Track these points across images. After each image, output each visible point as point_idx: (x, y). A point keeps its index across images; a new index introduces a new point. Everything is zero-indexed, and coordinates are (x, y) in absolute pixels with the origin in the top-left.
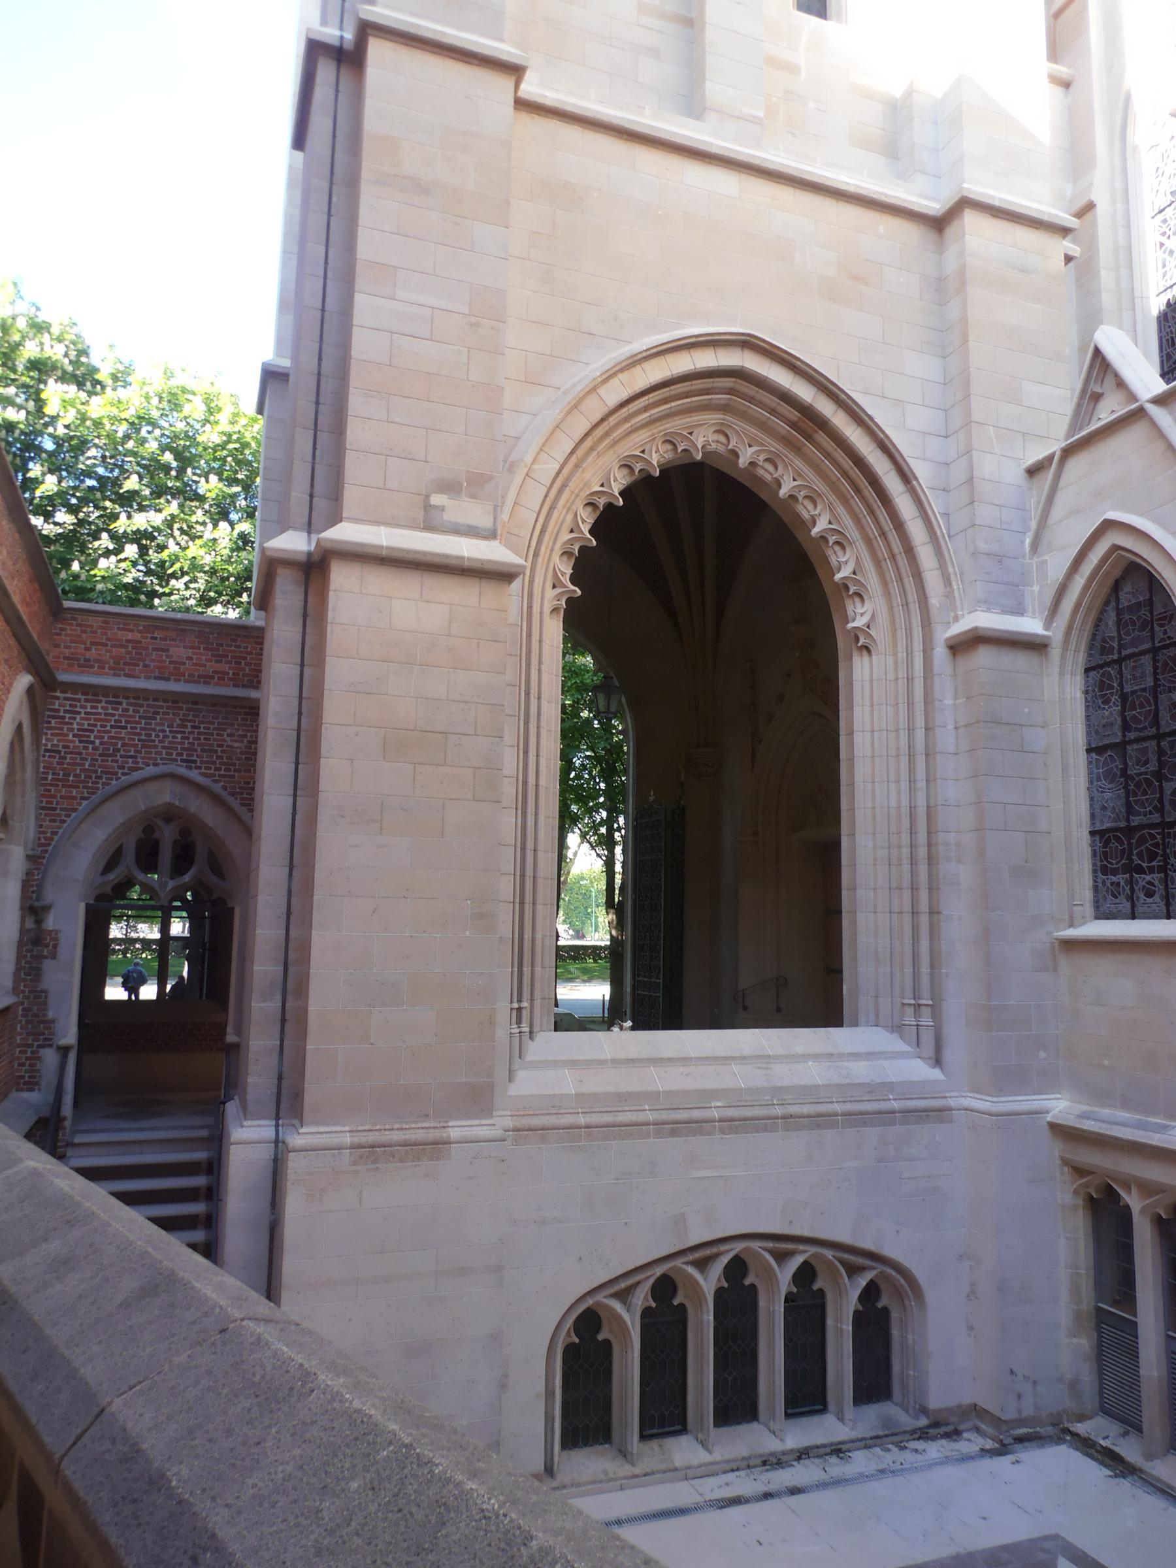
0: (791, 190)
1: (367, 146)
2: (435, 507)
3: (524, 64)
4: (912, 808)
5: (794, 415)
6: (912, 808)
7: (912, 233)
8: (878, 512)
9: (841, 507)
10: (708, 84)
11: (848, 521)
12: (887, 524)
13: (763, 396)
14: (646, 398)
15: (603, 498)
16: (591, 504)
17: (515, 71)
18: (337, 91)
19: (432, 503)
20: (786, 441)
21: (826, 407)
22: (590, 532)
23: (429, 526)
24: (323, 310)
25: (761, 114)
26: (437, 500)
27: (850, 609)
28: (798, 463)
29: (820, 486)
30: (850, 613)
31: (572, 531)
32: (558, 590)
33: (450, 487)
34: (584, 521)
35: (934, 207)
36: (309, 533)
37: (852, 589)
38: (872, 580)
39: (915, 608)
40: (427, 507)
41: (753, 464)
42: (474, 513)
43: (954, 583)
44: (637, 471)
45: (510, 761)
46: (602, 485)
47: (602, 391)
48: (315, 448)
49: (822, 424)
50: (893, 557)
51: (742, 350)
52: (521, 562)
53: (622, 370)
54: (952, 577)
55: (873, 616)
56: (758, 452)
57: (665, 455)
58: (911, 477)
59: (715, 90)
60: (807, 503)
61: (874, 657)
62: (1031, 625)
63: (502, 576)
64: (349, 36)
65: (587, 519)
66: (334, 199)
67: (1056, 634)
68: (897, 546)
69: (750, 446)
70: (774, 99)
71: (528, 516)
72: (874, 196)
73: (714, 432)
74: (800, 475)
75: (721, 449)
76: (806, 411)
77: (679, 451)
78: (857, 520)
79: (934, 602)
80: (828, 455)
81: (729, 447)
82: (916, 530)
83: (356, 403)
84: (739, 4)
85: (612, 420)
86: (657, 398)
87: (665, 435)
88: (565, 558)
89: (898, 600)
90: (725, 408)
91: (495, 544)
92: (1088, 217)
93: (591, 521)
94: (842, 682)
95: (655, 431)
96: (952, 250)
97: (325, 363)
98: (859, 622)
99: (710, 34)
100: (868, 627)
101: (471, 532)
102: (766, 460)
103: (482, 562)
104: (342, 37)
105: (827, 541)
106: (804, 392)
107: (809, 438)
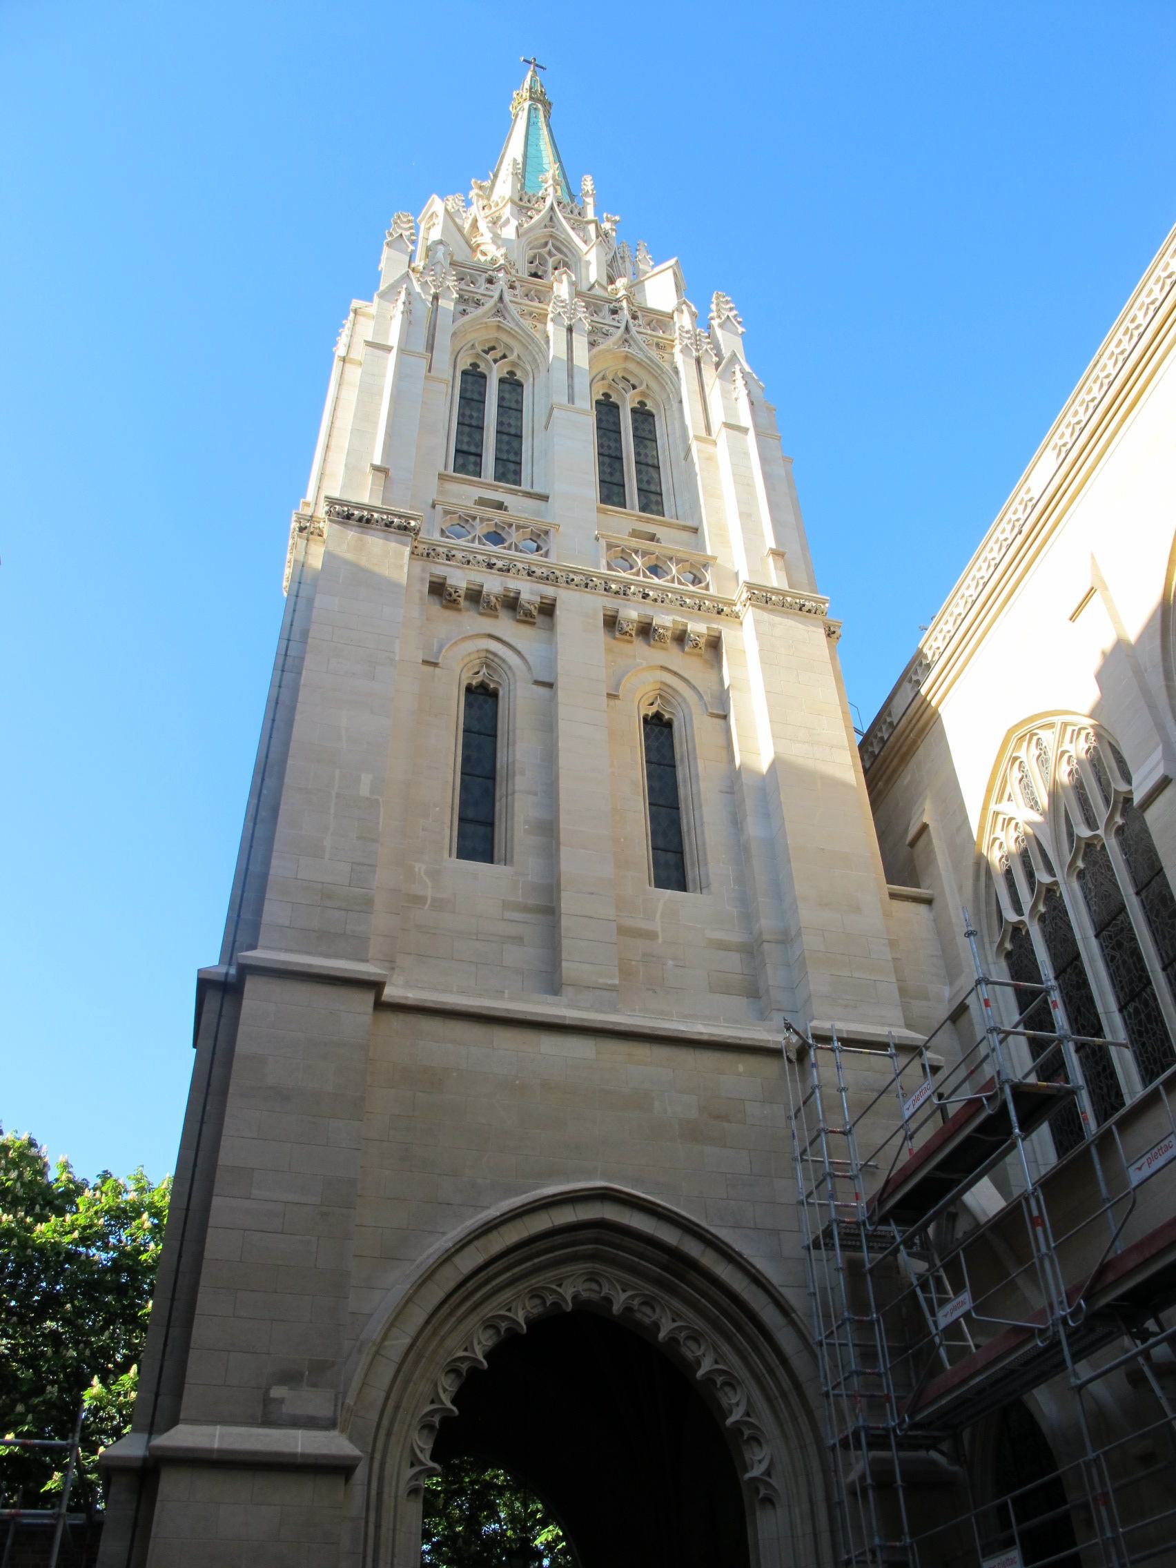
0: (648, 1045)
1: (236, 1065)
2: (275, 1400)
3: (381, 980)
5: (665, 1258)
9: (726, 1344)
10: (564, 964)
11: (734, 1359)
12: (774, 1360)
13: (628, 1242)
14: (506, 1259)
15: (466, 1364)
16: (453, 1370)
17: (376, 986)
18: (220, 1016)
19: (271, 1396)
20: (659, 1282)
21: (693, 1248)
22: (434, 1458)
23: (267, 1421)
24: (187, 1209)
25: (616, 982)
26: (277, 1392)
27: (747, 1456)
28: (676, 1304)
29: (700, 1324)
32: (417, 1469)
33: (290, 1378)
34: (445, 1390)
36: (150, 1434)
37: (747, 1433)
38: (765, 1419)
39: (803, 1419)
40: (267, 1401)
41: (628, 1309)
42: (315, 1402)
44: (503, 1331)
46: (466, 1350)
47: (457, 1260)
48: (165, 1345)
49: (693, 1265)
50: (784, 1395)
51: (602, 1202)
52: (356, 1452)
53: (477, 1237)
56: (632, 1297)
57: (532, 1311)
59: (569, 968)
60: (690, 1343)
63: (340, 1469)
64: (233, 971)
65: (447, 1388)
66: (208, 1108)
69: (624, 1291)
70: (633, 963)
71: (376, 1394)
72: (728, 1041)
74: (678, 1315)
75: (595, 1297)
76: (675, 1254)
80: (704, 1295)
81: (602, 1295)
83: (204, 1300)
84: (592, 894)
86: (501, 1267)
87: (532, 1290)
88: (425, 1432)
90: (592, 1257)
91: (334, 1433)
92: (963, 1021)
93: (453, 1389)
94: (751, 1543)
95: (521, 1287)
97: (183, 1260)
98: (757, 1472)
99: (565, 922)
101: (310, 1423)
102: (643, 1303)
103: (316, 1456)
104: (227, 974)
105: (714, 1382)
107: (682, 1279)
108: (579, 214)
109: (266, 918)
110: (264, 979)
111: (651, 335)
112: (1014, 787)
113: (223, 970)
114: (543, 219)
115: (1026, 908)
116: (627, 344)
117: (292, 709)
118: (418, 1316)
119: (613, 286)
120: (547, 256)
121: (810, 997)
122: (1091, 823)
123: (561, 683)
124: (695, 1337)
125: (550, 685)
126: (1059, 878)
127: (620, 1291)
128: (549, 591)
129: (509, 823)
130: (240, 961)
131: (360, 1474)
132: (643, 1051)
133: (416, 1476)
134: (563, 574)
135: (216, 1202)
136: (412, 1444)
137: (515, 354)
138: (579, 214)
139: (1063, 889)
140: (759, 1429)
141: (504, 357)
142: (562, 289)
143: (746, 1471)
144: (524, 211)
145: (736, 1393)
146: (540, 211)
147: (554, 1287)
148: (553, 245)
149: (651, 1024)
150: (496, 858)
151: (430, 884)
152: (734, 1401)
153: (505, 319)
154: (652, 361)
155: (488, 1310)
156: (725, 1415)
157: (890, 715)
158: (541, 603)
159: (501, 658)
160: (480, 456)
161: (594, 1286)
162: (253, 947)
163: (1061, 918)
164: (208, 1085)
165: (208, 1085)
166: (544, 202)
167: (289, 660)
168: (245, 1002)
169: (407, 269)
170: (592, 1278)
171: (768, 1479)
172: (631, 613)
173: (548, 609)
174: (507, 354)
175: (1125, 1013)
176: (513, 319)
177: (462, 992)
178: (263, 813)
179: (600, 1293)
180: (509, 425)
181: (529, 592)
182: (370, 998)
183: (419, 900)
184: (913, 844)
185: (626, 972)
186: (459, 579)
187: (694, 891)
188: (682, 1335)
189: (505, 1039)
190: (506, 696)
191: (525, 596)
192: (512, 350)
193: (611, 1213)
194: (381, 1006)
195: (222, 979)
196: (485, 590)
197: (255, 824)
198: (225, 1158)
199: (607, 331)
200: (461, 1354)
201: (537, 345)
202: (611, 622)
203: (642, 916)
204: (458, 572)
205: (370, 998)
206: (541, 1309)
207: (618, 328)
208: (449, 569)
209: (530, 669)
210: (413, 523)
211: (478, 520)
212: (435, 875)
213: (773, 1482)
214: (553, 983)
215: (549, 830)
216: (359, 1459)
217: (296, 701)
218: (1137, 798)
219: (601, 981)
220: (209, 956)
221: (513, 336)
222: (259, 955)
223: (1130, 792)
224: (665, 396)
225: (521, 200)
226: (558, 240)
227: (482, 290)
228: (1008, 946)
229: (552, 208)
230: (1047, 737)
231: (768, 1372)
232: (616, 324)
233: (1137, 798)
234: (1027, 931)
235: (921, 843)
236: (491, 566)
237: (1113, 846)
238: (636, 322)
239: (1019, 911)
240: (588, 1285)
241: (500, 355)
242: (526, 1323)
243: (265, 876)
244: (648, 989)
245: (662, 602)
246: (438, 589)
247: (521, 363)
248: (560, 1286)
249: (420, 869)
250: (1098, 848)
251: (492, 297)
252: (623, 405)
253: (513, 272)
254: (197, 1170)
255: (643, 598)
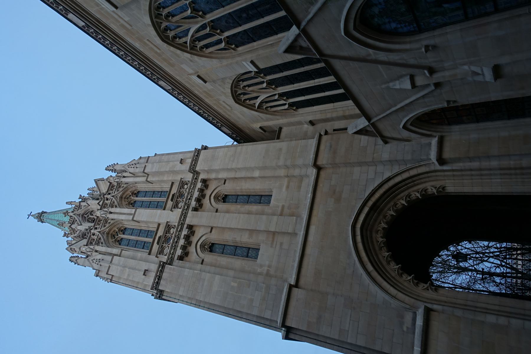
4: (501, 174)
6: (501, 174)
7: (322, 173)
8: (420, 178)
11: (402, 195)
12: (403, 183)
16: (401, 275)
17: (291, 287)
18: (296, 334)
21: (370, 203)
22: (426, 283)
28: (386, 209)
29: (392, 203)
30: (432, 193)
31: (410, 282)
35: (315, 171)
37: (424, 193)
39: (429, 175)
42: (408, 317)
43: (421, 164)
45: (491, 319)
49: (375, 204)
54: (419, 165)
55: (432, 186)
56: (383, 221)
58: (389, 178)
60: (397, 206)
61: (446, 186)
62: (434, 142)
63: (428, 312)
64: (283, 329)
67: (438, 134)
68: (410, 180)
69: (381, 224)
73: (378, 235)
76: (371, 209)
77: (383, 246)
78: (403, 191)
79: (427, 169)
82: (405, 175)
85: (377, 267)
89: (427, 179)
96: (326, 166)
100: (436, 187)
104: (284, 331)
106: (366, 210)
108: (77, 206)
109: (269, 318)
110: (286, 320)
111: (115, 190)
112: (252, 102)
113: (283, 331)
114: (77, 217)
115: (285, 102)
116: (117, 197)
117: (211, 304)
118: (385, 284)
119: (100, 199)
120: (89, 217)
121: (304, 164)
122: (263, 83)
123: (211, 225)
124: (395, 204)
125: (212, 228)
126: (277, 93)
127: (381, 225)
128: (185, 226)
129: (249, 243)
130: (281, 326)
131: (429, 306)
132: (315, 212)
133: (432, 289)
134: (181, 222)
135: (349, 341)
136: (423, 289)
137: (116, 229)
138: (77, 206)
139: (280, 92)
140: (422, 190)
141: (117, 232)
142: (98, 214)
143: (434, 194)
144: (74, 223)
145: (428, 189)
146: (75, 218)
147: (379, 243)
148: (85, 215)
149: (307, 209)
150: (259, 248)
151: (264, 268)
152: (414, 195)
153: (106, 231)
154: (123, 190)
155: (384, 263)
156: (418, 198)
157: (230, 134)
158: (188, 229)
159: (203, 242)
160: (145, 242)
161: (379, 232)
162: (277, 322)
163: (288, 93)
164: (315, 339)
165: (315, 339)
166: (72, 216)
167: (197, 304)
168: (293, 326)
169: (86, 259)
170: (377, 232)
171: (437, 188)
172: (193, 203)
173: (190, 227)
174: (116, 231)
175: (315, 78)
176: (106, 229)
177: (294, 261)
178: (240, 315)
179: (381, 230)
180: (137, 233)
181: (185, 232)
182: (295, 290)
183: (268, 270)
184: (265, 131)
185: (292, 215)
186: (179, 252)
187: (272, 193)
188: (395, 208)
189: (308, 251)
190: (214, 241)
191: (186, 233)
192: (115, 230)
193: (359, 225)
194: (297, 285)
195: (285, 332)
196: (183, 244)
197: (242, 318)
198: (336, 337)
199: (113, 202)
200: (396, 272)
201: (114, 223)
202: (195, 209)
203: (278, 209)
204: (177, 252)
205: (295, 290)
206: (385, 248)
207: (112, 199)
208: (176, 254)
209: (206, 233)
210: (162, 264)
211: (163, 245)
212: (261, 266)
213: (438, 186)
214: (294, 234)
215: (252, 232)
216: (425, 306)
217: (208, 303)
218: (256, 70)
219: (294, 222)
220: (279, 335)
221: (111, 229)
222: (279, 320)
223: (255, 71)
224: (134, 187)
225: (70, 223)
226: (84, 213)
227: (96, 237)
228: (295, 108)
229: (74, 214)
230: (240, 92)
231: (414, 182)
232: (111, 199)
233: (256, 70)
234: (291, 102)
235: (265, 129)
236: (177, 242)
237: (269, 78)
238: (111, 193)
239: (285, 104)
240: (379, 234)
241: (116, 234)
242: (398, 265)
243: (257, 316)
244: (298, 209)
245: (192, 194)
246: (181, 258)
247: (119, 228)
248: (379, 242)
249: (259, 270)
250: (269, 81)
251: (98, 235)
252: (135, 199)
253: (92, 228)
254: (340, 345)
255: (190, 200)
